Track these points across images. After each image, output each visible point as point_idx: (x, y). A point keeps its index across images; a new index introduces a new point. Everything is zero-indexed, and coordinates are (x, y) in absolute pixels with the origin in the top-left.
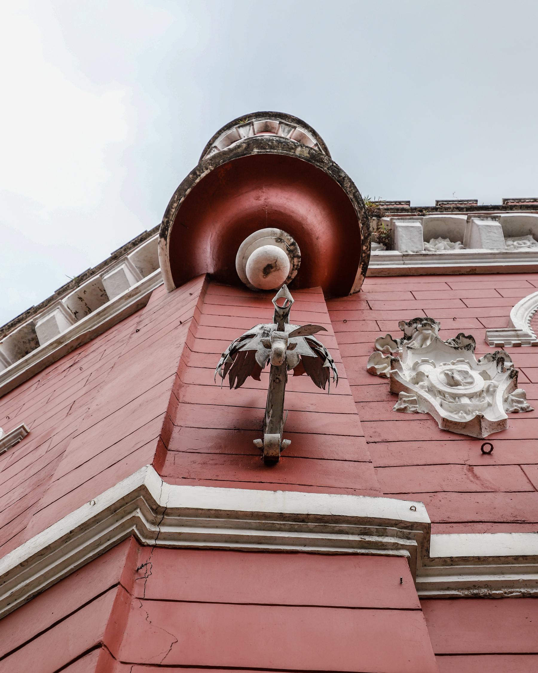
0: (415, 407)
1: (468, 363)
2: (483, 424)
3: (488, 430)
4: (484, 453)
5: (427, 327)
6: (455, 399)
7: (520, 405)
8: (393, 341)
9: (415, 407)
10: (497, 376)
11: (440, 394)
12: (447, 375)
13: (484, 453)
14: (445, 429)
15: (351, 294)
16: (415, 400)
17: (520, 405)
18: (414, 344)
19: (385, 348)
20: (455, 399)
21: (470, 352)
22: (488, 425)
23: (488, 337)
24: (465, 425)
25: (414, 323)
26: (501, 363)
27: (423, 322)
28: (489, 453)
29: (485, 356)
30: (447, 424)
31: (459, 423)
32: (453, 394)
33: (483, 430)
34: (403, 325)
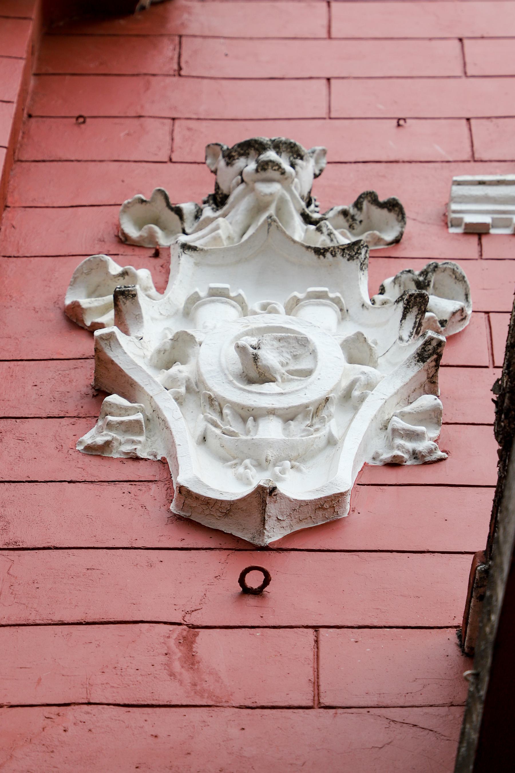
0: (133, 442)
1: (337, 301)
2: (272, 509)
3: (284, 524)
4: (247, 591)
5: (271, 173)
6: (244, 420)
7: (410, 445)
8: (172, 209)
9: (133, 442)
10: (395, 347)
11: (212, 405)
12: (241, 349)
13: (247, 591)
14: (182, 514)
15: (143, 8)
16: (138, 422)
17: (410, 445)
18: (217, 228)
19: (144, 233)
20: (244, 420)
21: (355, 264)
22: (289, 511)
23: (453, 199)
24: (228, 508)
25: (240, 155)
26: (415, 311)
27: (264, 157)
28: (258, 592)
29: (396, 278)
30: (189, 501)
31: (216, 501)
32: (243, 407)
33: (270, 523)
34: (215, 156)
